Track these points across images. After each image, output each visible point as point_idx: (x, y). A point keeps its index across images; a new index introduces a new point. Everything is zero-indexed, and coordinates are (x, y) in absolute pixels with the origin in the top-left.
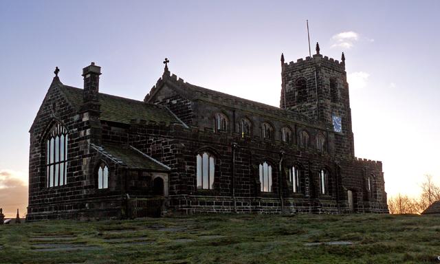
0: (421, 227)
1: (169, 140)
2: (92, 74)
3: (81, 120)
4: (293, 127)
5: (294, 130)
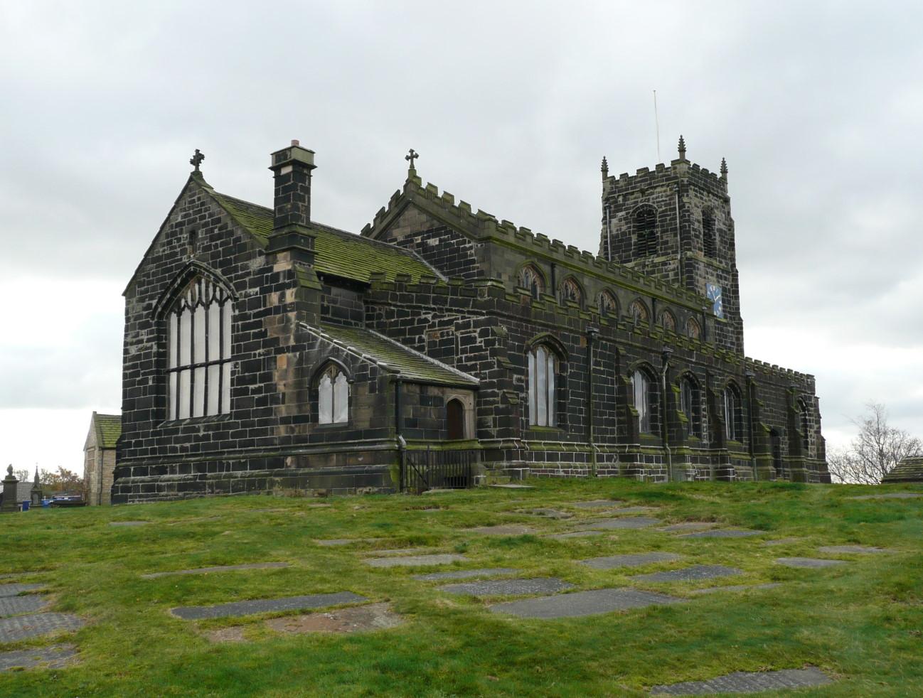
0: (373, 540)
2: (293, 171)
3: (271, 269)
4: (649, 302)
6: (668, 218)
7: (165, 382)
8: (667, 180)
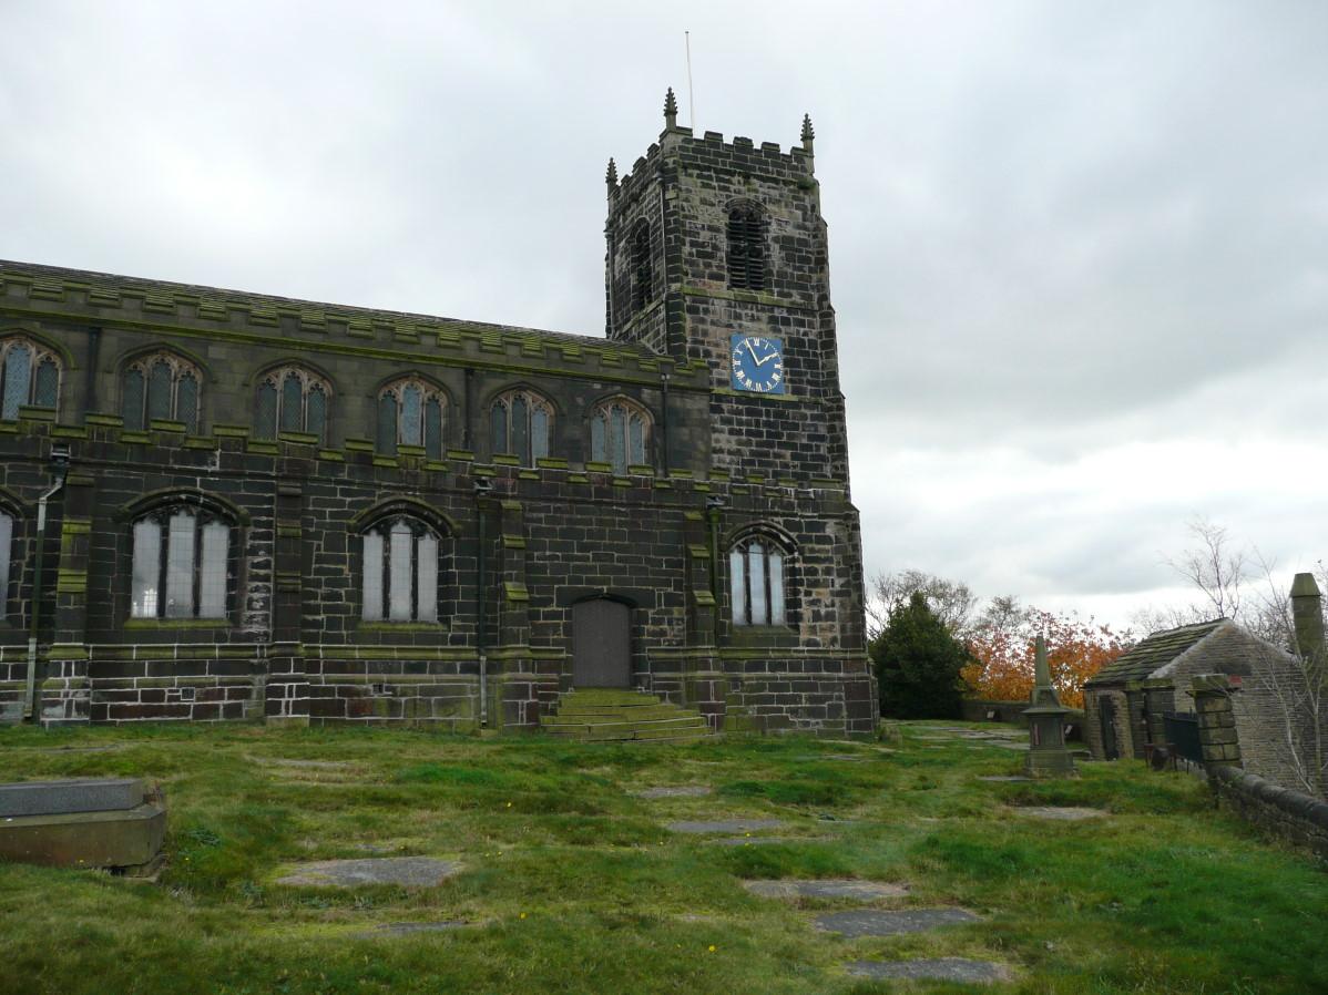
7: (789, 614)
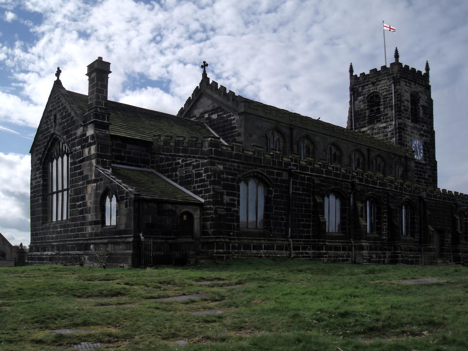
1: (201, 161)
2: (99, 71)
3: (85, 134)
5: (366, 154)
6: (388, 99)
8: (387, 76)
